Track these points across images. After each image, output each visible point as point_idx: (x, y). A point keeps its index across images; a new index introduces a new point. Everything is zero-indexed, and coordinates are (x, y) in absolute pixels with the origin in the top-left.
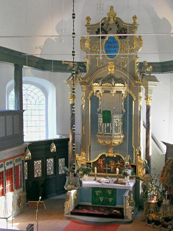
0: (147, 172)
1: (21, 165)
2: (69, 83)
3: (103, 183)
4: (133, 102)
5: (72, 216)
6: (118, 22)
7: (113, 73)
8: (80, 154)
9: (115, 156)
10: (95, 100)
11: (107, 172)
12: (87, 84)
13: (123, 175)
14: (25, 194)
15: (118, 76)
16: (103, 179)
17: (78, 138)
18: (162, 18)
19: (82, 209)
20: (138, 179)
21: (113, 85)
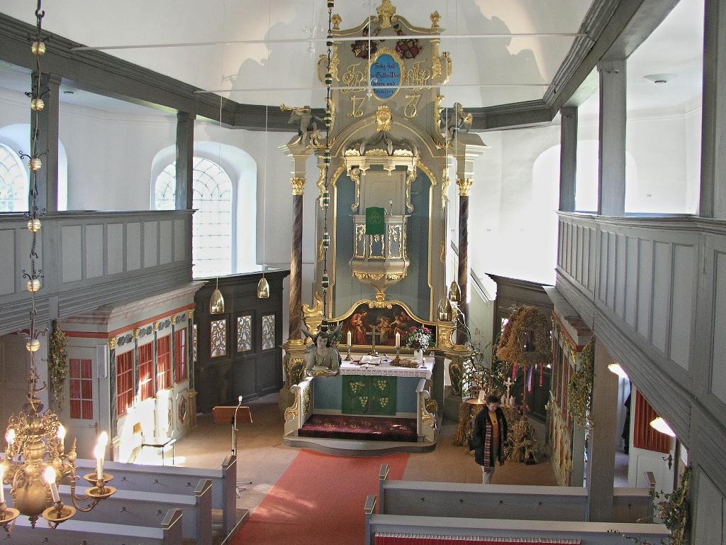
0: (462, 339)
1: (185, 329)
2: (292, 150)
3: (367, 365)
4: (431, 189)
5: (301, 440)
6: (398, 27)
7: (387, 128)
8: (313, 303)
9: (390, 307)
10: (346, 185)
11: (374, 342)
12: (330, 155)
13: (411, 346)
14: (193, 393)
15: (398, 136)
16: (365, 358)
17: (309, 272)
18: (490, 18)
19: (322, 424)
20: (440, 356)
21: (391, 153)
